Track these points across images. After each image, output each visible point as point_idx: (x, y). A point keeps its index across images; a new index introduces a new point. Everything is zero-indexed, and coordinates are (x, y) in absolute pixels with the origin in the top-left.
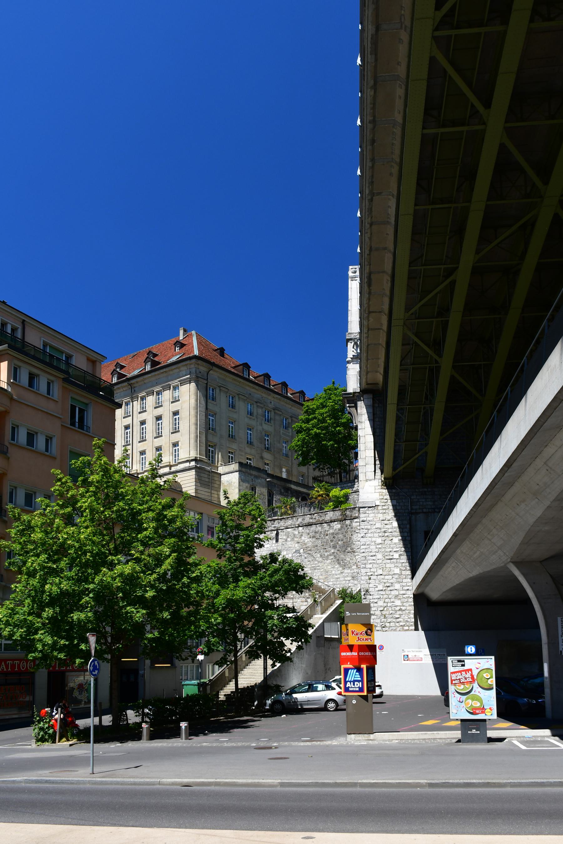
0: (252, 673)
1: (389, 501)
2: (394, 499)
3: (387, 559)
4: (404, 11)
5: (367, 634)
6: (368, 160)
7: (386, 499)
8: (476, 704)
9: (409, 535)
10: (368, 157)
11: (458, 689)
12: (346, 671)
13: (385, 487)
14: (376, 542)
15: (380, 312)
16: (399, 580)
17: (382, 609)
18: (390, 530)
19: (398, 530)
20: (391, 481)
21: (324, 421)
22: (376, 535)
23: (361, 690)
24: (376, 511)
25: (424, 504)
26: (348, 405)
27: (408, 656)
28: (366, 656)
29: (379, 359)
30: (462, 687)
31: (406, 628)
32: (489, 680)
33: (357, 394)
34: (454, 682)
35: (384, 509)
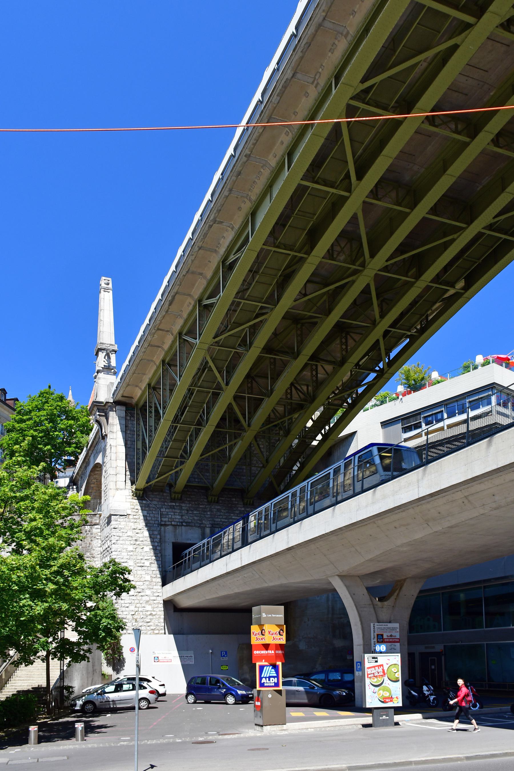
0: (27, 675)
1: (140, 511)
2: (145, 510)
3: (138, 566)
4: (323, 70)
5: (262, 635)
6: (227, 189)
7: (137, 509)
8: (386, 694)
9: (159, 545)
10: (228, 187)
11: (372, 682)
12: (262, 668)
13: (136, 498)
14: (128, 550)
15: (168, 331)
16: (150, 587)
17: (133, 613)
18: (141, 539)
19: (149, 539)
20: (141, 492)
21: (40, 423)
22: (128, 542)
23: (277, 685)
24: (127, 519)
25: (173, 517)
26: (98, 413)
27: (158, 657)
28: (262, 654)
29: (144, 374)
30: (376, 680)
31: (157, 632)
32: (396, 674)
33: (110, 404)
34: (369, 676)
35: (135, 519)
